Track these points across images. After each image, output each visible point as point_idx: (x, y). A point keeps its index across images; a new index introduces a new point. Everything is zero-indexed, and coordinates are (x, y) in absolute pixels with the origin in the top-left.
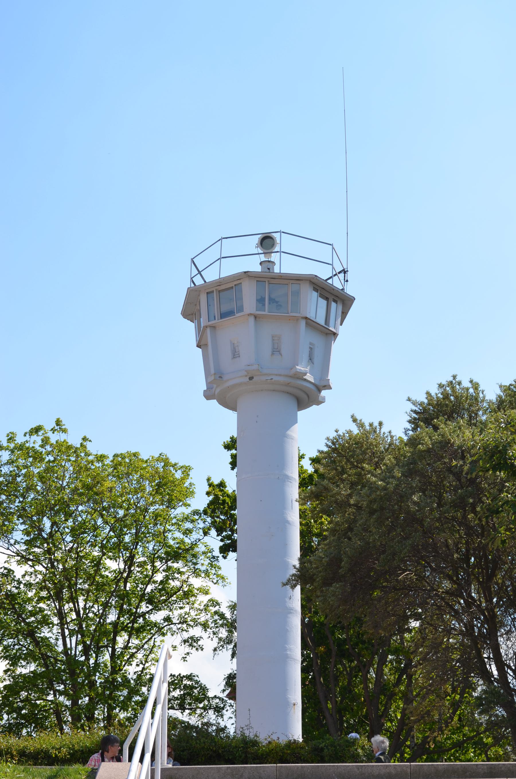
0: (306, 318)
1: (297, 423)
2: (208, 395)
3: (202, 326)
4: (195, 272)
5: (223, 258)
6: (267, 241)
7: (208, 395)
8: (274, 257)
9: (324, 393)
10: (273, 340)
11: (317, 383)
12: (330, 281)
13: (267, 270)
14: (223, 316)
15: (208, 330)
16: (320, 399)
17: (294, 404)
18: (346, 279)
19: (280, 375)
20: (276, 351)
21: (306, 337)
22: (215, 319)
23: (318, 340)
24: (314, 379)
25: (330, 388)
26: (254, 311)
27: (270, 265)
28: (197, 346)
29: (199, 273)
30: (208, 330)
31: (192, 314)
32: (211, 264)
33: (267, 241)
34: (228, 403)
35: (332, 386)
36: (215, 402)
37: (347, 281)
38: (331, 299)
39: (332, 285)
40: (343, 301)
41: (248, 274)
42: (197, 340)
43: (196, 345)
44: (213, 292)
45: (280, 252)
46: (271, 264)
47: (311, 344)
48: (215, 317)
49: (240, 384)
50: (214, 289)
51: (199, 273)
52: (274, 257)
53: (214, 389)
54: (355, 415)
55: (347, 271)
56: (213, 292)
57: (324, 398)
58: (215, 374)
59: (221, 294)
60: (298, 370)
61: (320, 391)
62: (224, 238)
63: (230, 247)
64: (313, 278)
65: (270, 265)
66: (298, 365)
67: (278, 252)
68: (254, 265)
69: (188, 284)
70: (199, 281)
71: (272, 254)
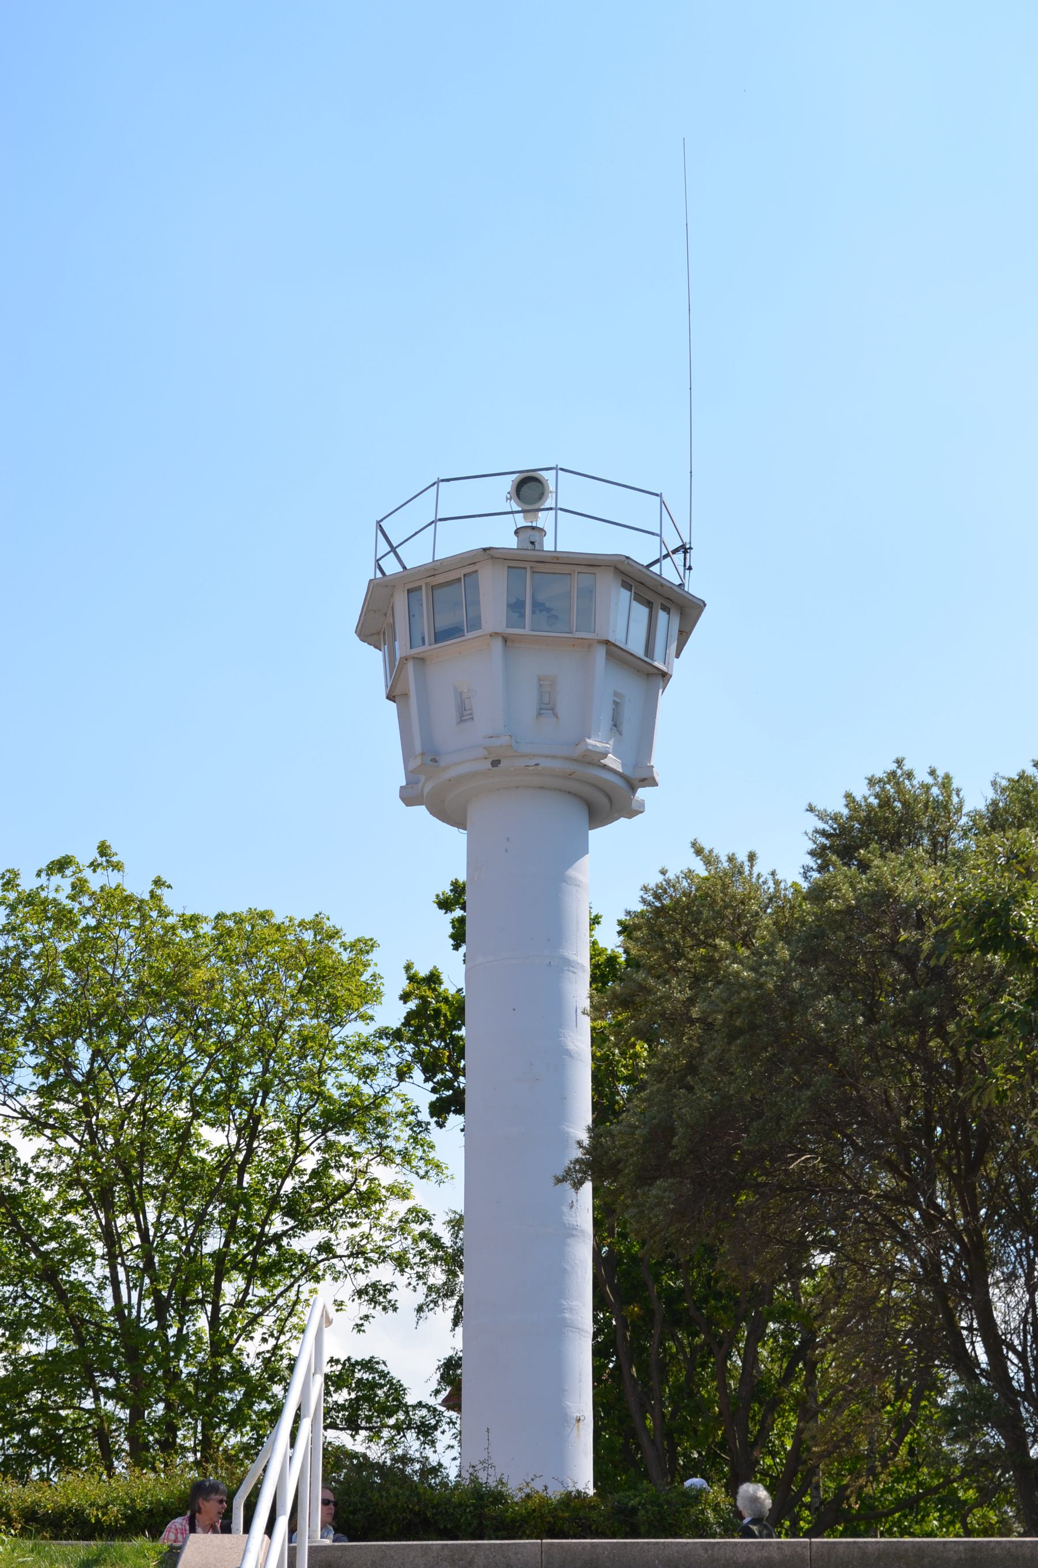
0: (607, 642)
1: (587, 853)
2: (409, 797)
3: (398, 657)
4: (384, 547)
5: (440, 520)
6: (529, 488)
7: (409, 797)
8: (544, 520)
9: (642, 793)
10: (541, 686)
11: (628, 773)
12: (655, 569)
13: (530, 546)
14: (440, 636)
15: (410, 666)
16: (634, 806)
17: (581, 815)
18: (688, 565)
19: (554, 757)
20: (546, 708)
21: (606, 680)
22: (424, 643)
23: (630, 687)
24: (623, 765)
25: (657, 785)
26: (502, 628)
27: (535, 536)
28: (388, 698)
29: (393, 549)
30: (410, 666)
31: (378, 633)
32: (416, 533)
33: (529, 488)
34: (450, 813)
35: (657, 778)
36: (422, 810)
37: (690, 568)
38: (657, 605)
39: (660, 576)
40: (682, 609)
41: (491, 552)
42: (387, 686)
43: (384, 696)
44: (419, 588)
45: (556, 509)
46: (536, 533)
47: (616, 694)
48: (423, 639)
49: (474, 775)
50: (422, 583)
51: (393, 549)
52: (544, 520)
53: (420, 785)
54: (699, 841)
55: (690, 548)
56: (419, 588)
57: (642, 804)
58: (423, 754)
59: (436, 592)
60: (590, 747)
61: (633, 789)
62: (443, 481)
63: (455, 499)
64: (622, 562)
65: (535, 536)
66: (589, 738)
67: (551, 509)
68: (502, 535)
69: (369, 573)
70: (391, 567)
71: (540, 514)
